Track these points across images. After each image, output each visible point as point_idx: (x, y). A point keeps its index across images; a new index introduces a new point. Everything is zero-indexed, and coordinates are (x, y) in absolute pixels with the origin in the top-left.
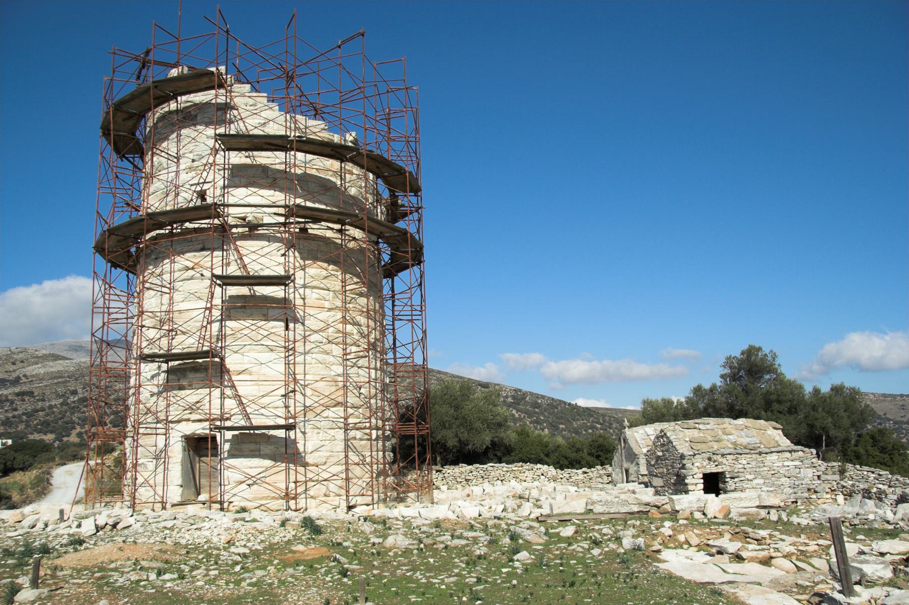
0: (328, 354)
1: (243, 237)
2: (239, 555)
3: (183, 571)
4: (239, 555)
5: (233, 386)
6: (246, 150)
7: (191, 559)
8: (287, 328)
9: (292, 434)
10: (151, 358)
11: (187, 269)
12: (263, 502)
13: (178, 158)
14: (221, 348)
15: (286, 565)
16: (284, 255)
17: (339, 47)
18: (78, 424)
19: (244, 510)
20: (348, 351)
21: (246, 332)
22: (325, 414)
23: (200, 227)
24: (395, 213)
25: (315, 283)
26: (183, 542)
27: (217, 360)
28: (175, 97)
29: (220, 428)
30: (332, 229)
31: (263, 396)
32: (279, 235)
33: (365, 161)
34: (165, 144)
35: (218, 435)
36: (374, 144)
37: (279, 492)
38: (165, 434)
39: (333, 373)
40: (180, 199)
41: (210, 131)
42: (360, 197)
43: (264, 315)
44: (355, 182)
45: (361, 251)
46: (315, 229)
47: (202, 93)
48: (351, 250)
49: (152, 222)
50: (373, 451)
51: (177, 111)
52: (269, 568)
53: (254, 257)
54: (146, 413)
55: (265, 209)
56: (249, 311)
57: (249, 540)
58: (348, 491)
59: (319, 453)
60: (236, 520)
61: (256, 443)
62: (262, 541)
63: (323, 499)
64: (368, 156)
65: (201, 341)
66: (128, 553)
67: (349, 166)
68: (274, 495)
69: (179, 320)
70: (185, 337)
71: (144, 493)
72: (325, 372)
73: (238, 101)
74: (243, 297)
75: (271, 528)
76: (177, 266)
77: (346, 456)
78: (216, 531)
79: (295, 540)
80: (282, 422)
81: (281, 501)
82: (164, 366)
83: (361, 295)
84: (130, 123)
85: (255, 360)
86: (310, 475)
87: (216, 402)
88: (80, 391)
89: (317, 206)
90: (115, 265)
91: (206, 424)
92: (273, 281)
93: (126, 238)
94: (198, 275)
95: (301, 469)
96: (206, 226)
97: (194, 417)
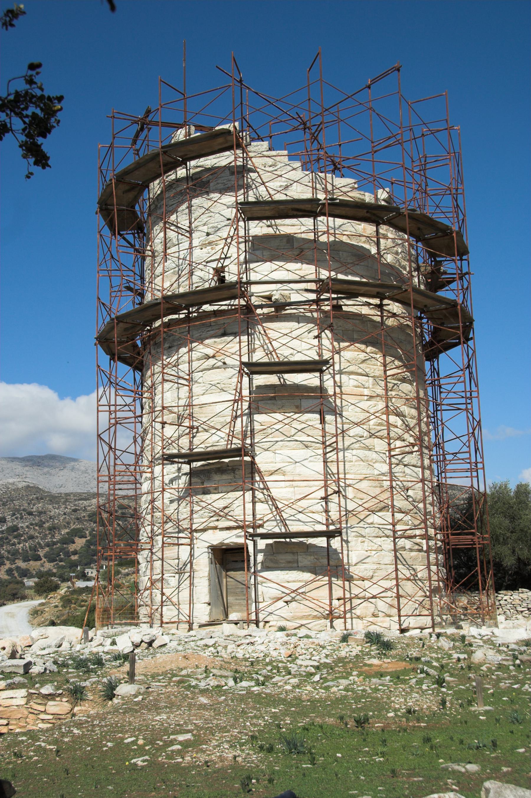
0: (370, 450)
1: (269, 318)
2: (311, 666)
6: (268, 218)
8: (323, 421)
9: (336, 543)
10: (169, 459)
11: (208, 357)
12: (304, 622)
13: (191, 232)
14: (251, 445)
16: (318, 337)
17: (369, 87)
18: (8, 559)
20: (392, 446)
21: (277, 427)
22: (369, 520)
23: (223, 308)
24: (436, 281)
25: (352, 368)
27: (247, 459)
28: (183, 163)
29: (253, 535)
30: (369, 304)
31: (300, 500)
32: (309, 314)
33: (407, 223)
34: (173, 218)
35: (250, 544)
36: (407, 200)
37: (321, 610)
38: (190, 545)
39: (376, 472)
40: (195, 279)
41: (229, 199)
42: (397, 265)
43: (297, 407)
44: (391, 247)
45: (402, 328)
46: (350, 306)
47: (214, 156)
48: (392, 328)
49: (168, 306)
50: (425, 566)
51: (187, 178)
53: (284, 340)
55: (292, 286)
56: (279, 402)
58: (399, 610)
59: (365, 566)
61: (293, 553)
63: (371, 619)
64: (411, 217)
65: (230, 439)
66: (193, 662)
67: (384, 229)
68: (316, 613)
69: (201, 416)
71: (169, 613)
72: (367, 471)
73: (258, 162)
76: (195, 355)
77: (397, 570)
78: (272, 646)
80: (323, 528)
81: (323, 621)
82: (186, 468)
83: (404, 380)
84: (131, 195)
86: (356, 591)
88: (8, 518)
89: (350, 278)
93: (135, 325)
94: (220, 364)
96: (225, 308)
97: (223, 524)
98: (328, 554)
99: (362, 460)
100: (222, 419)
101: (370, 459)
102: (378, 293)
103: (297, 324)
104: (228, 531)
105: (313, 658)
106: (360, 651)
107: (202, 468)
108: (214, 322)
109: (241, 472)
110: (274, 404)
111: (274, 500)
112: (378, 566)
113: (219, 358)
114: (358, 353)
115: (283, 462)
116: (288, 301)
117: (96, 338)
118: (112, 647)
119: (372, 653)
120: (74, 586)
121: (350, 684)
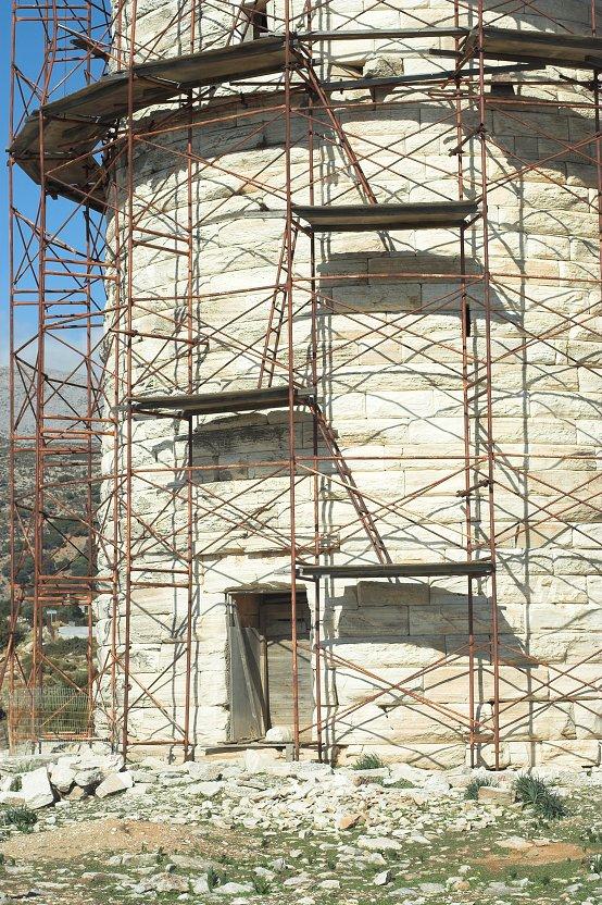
1: (358, 112)
2: (380, 851)
3: (262, 879)
4: (380, 851)
5: (345, 473)
7: (275, 856)
10: (148, 407)
15: (487, 875)
16: (457, 152)
19: (371, 763)
21: (372, 340)
26: (250, 823)
29: (316, 573)
30: (573, 81)
31: (414, 495)
35: (310, 587)
37: (455, 725)
38: (188, 586)
43: (413, 300)
49: (144, 85)
52: (451, 880)
53: (385, 159)
54: (143, 538)
57: (396, 825)
60: (362, 781)
61: (399, 607)
62: (427, 827)
65: (268, 366)
66: (140, 838)
68: (443, 730)
70: (228, 355)
71: (144, 723)
74: (363, 258)
75: (445, 801)
76: (206, 188)
78: (321, 803)
79: (502, 827)
80: (460, 556)
85: (396, 406)
87: (306, 513)
90: (53, 189)
91: (285, 561)
92: (433, 216)
93: (83, 126)
95: (507, 671)
96: (272, 89)
98: (471, 609)
99: (553, 413)
100: (256, 326)
101: (567, 411)
102: (588, 58)
103: (416, 123)
104: (266, 560)
105: (395, 833)
106: (497, 819)
107: (216, 427)
108: (245, 118)
109: (291, 438)
110: (364, 293)
111: (360, 496)
112: (579, 635)
113: (254, 196)
114: (546, 185)
115: (382, 417)
116: (399, 74)
117: (10, 151)
118: (14, 794)
119: (521, 822)
120: (53, 635)
121: (441, 895)
